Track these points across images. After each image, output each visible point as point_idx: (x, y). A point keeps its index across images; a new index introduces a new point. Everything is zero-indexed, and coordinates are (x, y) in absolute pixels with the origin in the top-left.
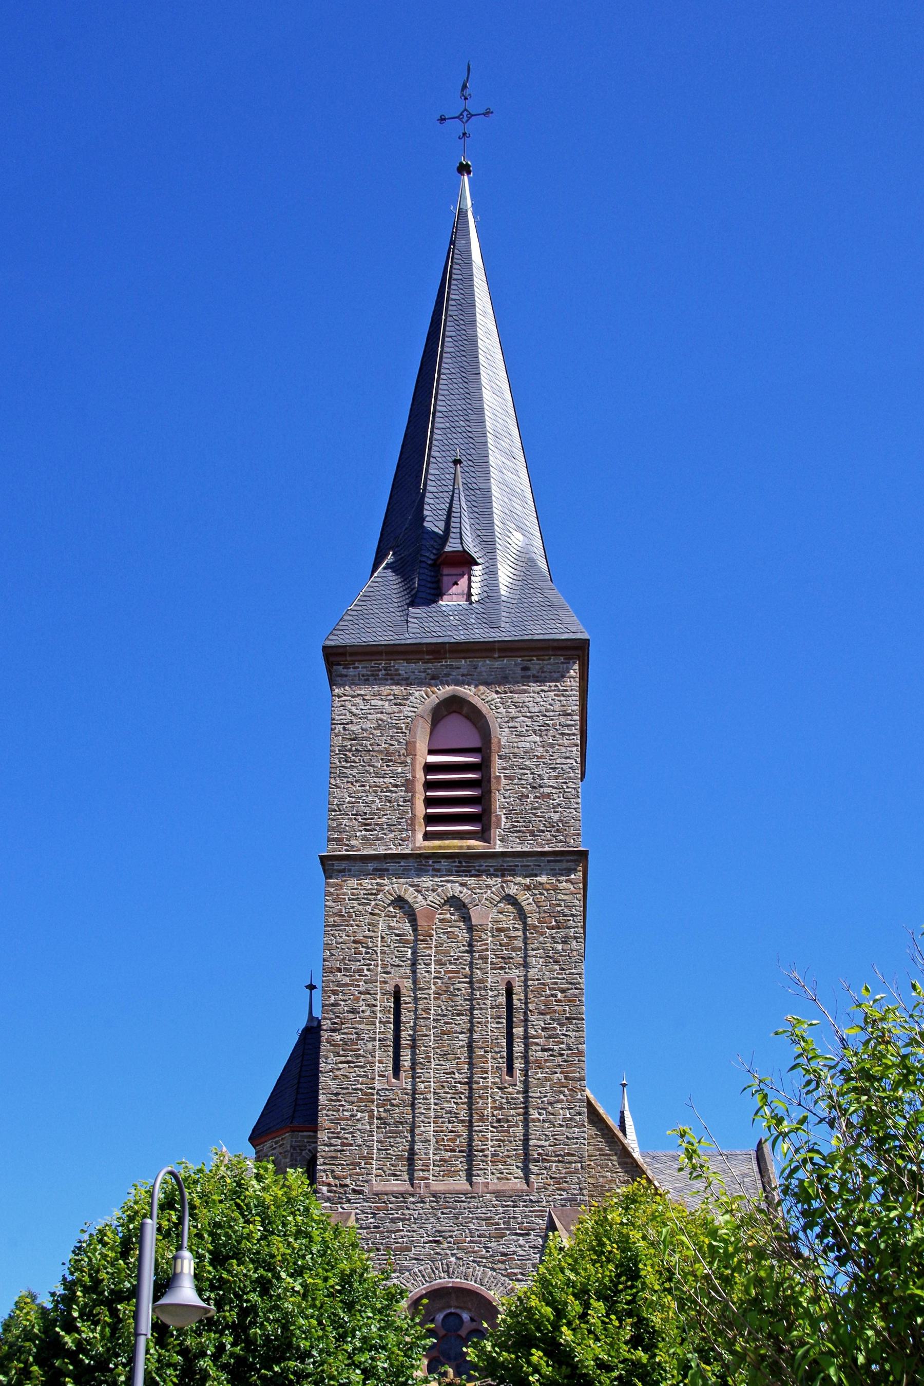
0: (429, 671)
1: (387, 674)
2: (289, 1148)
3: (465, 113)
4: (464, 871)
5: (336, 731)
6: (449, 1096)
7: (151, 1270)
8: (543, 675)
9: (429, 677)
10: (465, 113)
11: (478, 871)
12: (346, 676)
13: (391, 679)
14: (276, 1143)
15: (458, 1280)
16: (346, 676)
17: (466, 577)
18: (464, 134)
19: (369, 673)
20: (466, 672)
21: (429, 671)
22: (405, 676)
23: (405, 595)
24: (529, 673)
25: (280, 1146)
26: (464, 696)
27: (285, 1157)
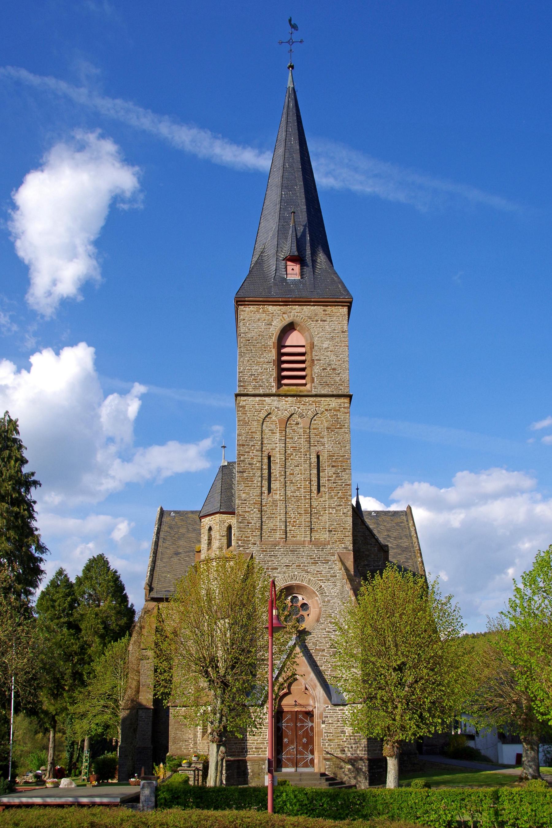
0: (282, 310)
1: (263, 311)
2: (218, 521)
3: (291, 43)
4: (298, 402)
5: (241, 336)
6: (293, 502)
7: (83, 789)
8: (333, 314)
9: (282, 313)
10: (291, 43)
11: (305, 402)
12: (245, 311)
13: (266, 313)
14: (212, 518)
15: (298, 582)
16: (245, 311)
17: (298, 237)
18: (291, 50)
19: (255, 310)
20: (298, 311)
21: (282, 310)
22: (272, 312)
23: (210, 600)
24: (327, 313)
25: (214, 520)
26: (298, 585)
27: (217, 525)
